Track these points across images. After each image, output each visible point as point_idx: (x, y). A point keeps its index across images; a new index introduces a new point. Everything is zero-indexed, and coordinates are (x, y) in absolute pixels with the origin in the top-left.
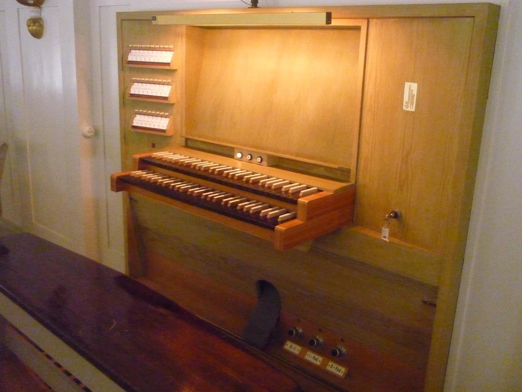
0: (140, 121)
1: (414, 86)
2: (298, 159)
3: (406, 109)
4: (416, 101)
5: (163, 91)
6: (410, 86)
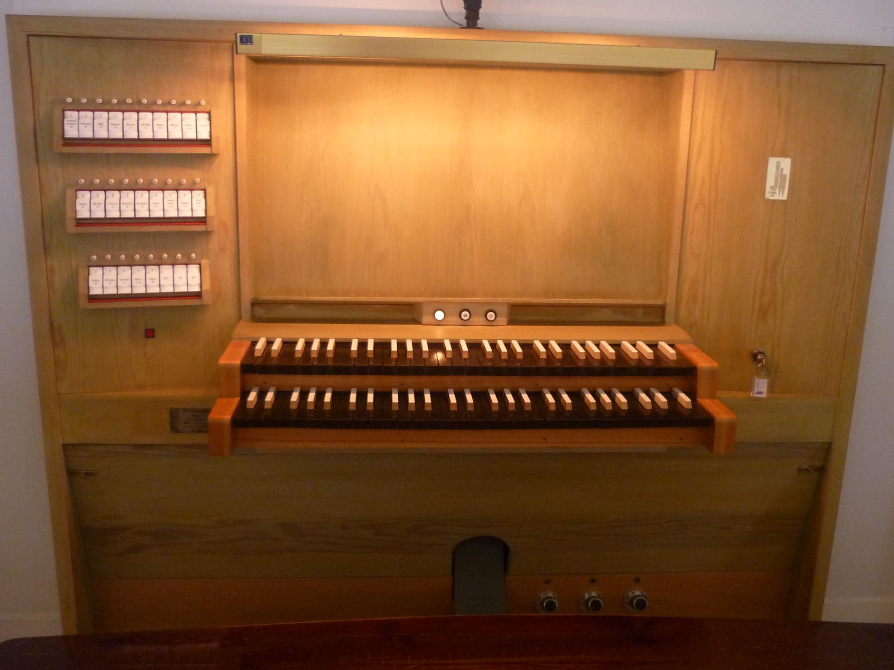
0: (105, 281)
1: (786, 164)
2: (573, 301)
3: (772, 198)
4: (790, 187)
5: (189, 204)
6: (778, 163)
